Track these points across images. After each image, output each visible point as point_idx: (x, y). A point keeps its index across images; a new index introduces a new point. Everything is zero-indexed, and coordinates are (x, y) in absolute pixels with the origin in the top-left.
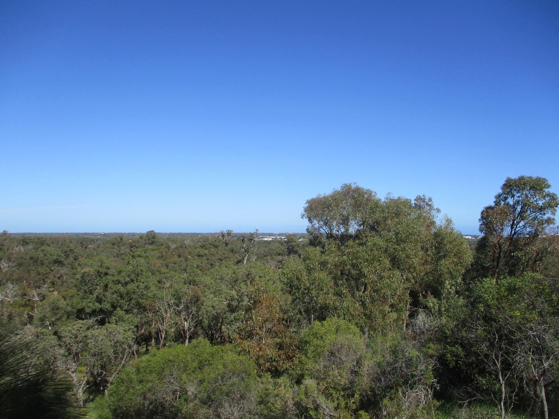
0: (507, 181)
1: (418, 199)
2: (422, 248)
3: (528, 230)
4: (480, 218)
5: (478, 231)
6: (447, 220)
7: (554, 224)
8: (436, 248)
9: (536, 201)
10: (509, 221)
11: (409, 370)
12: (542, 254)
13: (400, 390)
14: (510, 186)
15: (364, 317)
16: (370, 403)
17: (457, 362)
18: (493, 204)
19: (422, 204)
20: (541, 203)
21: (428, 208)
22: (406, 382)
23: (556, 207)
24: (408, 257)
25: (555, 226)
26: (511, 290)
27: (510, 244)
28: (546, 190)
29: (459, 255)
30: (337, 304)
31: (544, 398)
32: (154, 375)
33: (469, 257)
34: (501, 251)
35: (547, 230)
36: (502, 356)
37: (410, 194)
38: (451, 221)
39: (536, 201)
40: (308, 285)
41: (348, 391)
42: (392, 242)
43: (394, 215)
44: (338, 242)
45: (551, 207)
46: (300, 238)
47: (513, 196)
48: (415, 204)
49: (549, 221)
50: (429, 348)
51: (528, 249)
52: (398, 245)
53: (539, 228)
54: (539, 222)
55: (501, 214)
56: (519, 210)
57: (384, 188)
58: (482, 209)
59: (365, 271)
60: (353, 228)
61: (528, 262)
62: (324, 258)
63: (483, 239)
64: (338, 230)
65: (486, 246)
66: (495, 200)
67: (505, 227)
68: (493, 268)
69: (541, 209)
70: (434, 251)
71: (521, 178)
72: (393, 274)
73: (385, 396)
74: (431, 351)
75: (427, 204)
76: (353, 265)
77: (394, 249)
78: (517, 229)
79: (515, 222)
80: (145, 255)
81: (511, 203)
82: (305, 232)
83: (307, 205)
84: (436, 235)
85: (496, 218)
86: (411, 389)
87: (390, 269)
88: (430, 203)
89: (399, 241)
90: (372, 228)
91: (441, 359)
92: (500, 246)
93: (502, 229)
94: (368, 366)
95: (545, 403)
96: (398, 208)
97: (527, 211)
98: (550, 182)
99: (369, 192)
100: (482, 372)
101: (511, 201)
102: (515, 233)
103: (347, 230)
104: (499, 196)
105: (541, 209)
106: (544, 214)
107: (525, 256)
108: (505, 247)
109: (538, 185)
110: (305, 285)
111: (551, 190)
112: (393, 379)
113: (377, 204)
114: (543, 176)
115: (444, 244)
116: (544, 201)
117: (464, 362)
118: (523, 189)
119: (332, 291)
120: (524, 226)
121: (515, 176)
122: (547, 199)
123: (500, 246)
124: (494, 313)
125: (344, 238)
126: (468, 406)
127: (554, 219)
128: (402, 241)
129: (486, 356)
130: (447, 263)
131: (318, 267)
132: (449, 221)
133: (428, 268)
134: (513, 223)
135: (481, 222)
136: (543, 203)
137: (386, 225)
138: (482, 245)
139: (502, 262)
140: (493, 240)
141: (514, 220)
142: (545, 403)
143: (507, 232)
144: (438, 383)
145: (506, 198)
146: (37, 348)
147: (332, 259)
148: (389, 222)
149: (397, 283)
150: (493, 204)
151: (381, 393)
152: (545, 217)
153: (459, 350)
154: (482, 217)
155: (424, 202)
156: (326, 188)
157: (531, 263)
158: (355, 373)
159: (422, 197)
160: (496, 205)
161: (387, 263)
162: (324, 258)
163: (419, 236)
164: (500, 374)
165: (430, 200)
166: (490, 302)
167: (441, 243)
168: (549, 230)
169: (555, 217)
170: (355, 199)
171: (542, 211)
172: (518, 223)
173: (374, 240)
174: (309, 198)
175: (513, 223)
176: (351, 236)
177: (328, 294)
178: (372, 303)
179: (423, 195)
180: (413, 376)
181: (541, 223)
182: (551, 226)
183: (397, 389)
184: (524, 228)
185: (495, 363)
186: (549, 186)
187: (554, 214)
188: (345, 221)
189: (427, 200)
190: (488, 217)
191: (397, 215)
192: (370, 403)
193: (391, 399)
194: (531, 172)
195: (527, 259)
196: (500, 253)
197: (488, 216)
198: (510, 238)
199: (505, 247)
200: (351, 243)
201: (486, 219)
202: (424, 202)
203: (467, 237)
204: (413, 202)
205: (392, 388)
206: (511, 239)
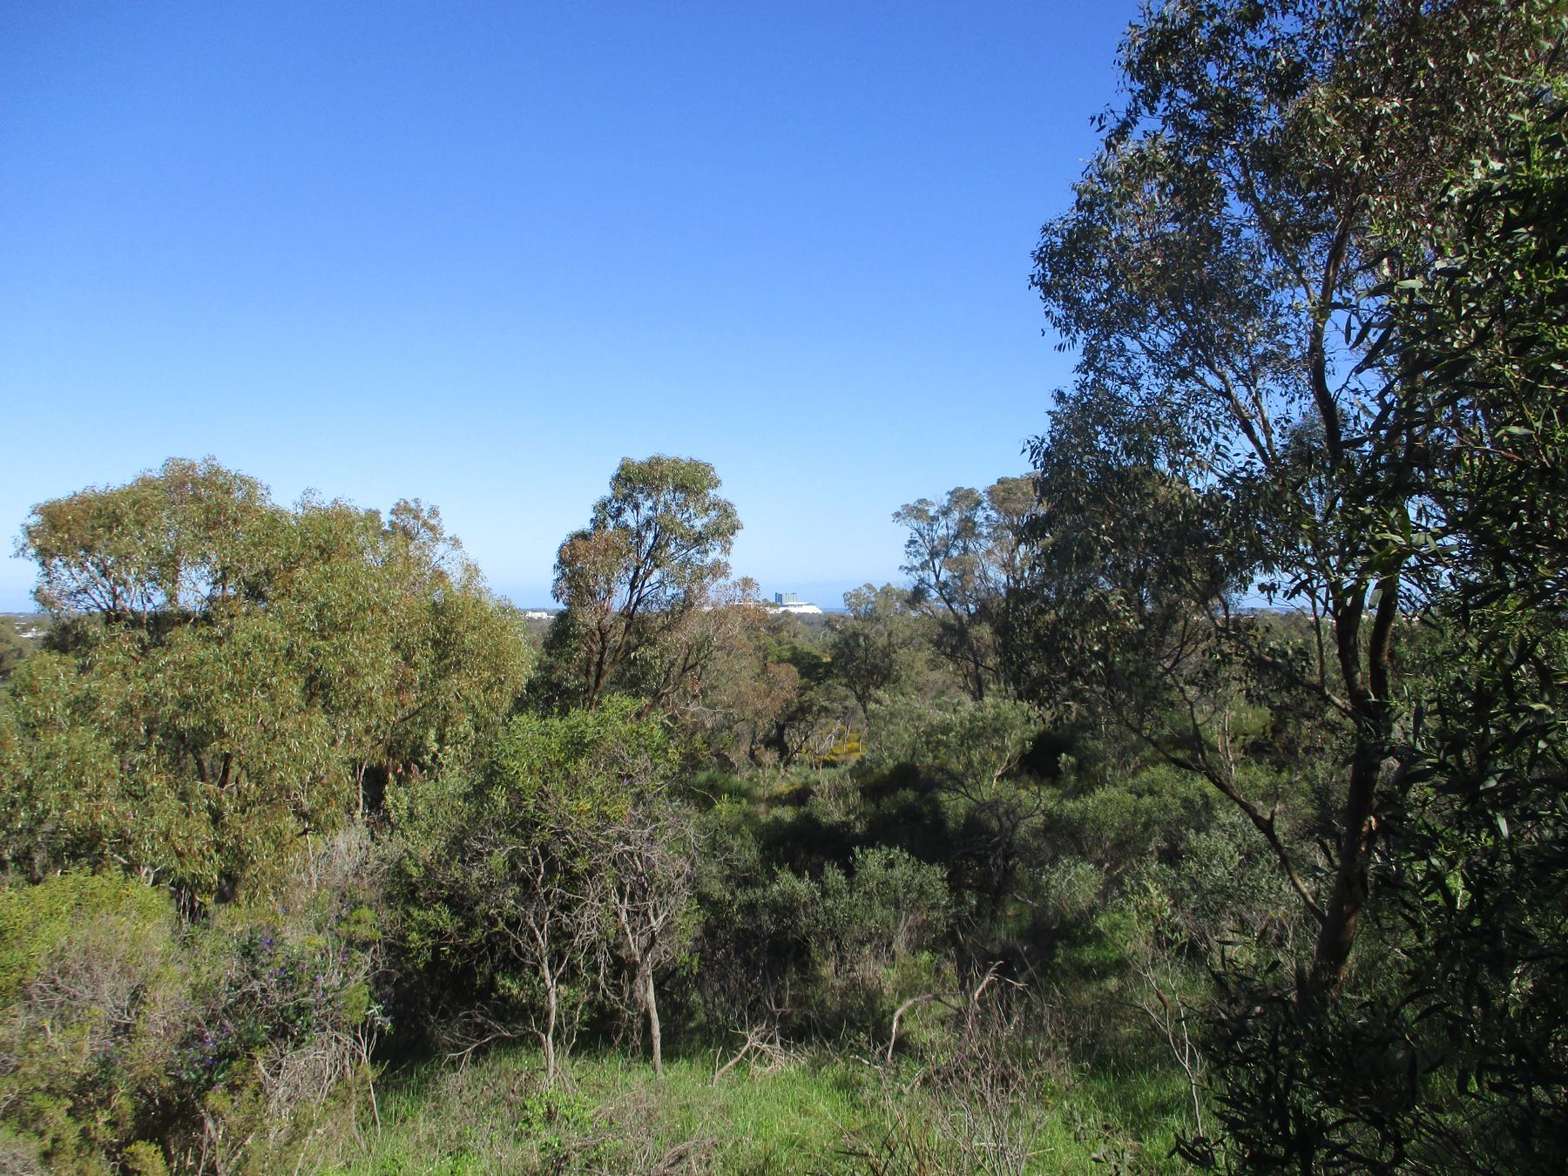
0: (622, 468)
1: (401, 509)
2: (396, 648)
3: (670, 591)
4: (555, 561)
5: (550, 596)
6: (467, 569)
7: (727, 577)
8: (436, 643)
9: (689, 520)
10: (627, 569)
11: (290, 995)
12: (699, 650)
13: (259, 1054)
14: (633, 481)
15: (217, 857)
16: (169, 1118)
17: (436, 950)
18: (588, 526)
19: (410, 526)
20: (698, 524)
21: (431, 534)
22: (281, 1032)
24: (351, 671)
25: (729, 583)
26: (577, 747)
27: (628, 627)
28: (712, 492)
29: (497, 662)
30: (130, 826)
31: (653, 1005)
33: (524, 666)
34: (604, 648)
36: (552, 915)
37: (373, 494)
38: (477, 571)
39: (689, 520)
40: (27, 773)
41: (86, 1093)
42: (307, 630)
43: (316, 553)
44: (144, 634)
46: (25, 630)
47: (637, 507)
48: (392, 524)
49: (718, 570)
50: (358, 922)
51: (669, 639)
52: (324, 638)
53: (695, 587)
55: (606, 550)
56: (650, 541)
57: (295, 473)
58: (561, 537)
59: (225, 715)
60: (194, 588)
61: (667, 673)
62: (89, 684)
63: (562, 616)
64: (145, 599)
65: (567, 636)
66: (593, 516)
67: (616, 586)
68: (586, 691)
69: (699, 539)
70: (430, 652)
71: (655, 462)
72: (310, 724)
73: (211, 1084)
74: (363, 932)
75: (425, 524)
76: (186, 704)
77: (312, 651)
78: (645, 591)
79: (641, 571)
81: (633, 524)
82: (31, 607)
83: (36, 519)
84: (437, 610)
85: (594, 563)
86: (296, 1047)
87: (301, 710)
88: (433, 522)
89: (327, 627)
90: (254, 592)
91: (397, 949)
92: (603, 636)
93: (609, 591)
94: (169, 1003)
95: (654, 1015)
96: (328, 536)
97: (667, 545)
98: (720, 472)
99: (249, 484)
100: (513, 965)
101: (630, 518)
102: (639, 601)
103: (172, 598)
104: (603, 506)
105: (699, 539)
107: (662, 656)
108: (616, 638)
109: (691, 481)
110: (16, 774)
111: (721, 494)
112: (252, 1024)
113: (275, 519)
114: (702, 456)
115: (458, 634)
116: (706, 520)
117: (456, 948)
118: (658, 489)
119: (111, 788)
120: (661, 582)
121: (640, 455)
123: (603, 636)
124: (531, 808)
125: (160, 624)
126: (475, 1062)
127: (727, 565)
128: (335, 627)
129: (513, 924)
130: (464, 684)
131: (61, 714)
132: (472, 571)
133: (412, 699)
134: (636, 573)
135: (558, 574)
137: (292, 581)
138: (561, 633)
139: (610, 672)
140: (587, 618)
141: (638, 569)
142: (654, 1015)
143: (620, 597)
144: (385, 1013)
145: (620, 511)
147: (111, 692)
148: (301, 572)
149: (324, 748)
150: (588, 526)
151: (199, 1078)
152: (709, 560)
153: (442, 917)
154: (562, 561)
155: (416, 517)
156: (111, 466)
157: (675, 671)
158: (124, 1030)
159: (413, 505)
160: (596, 527)
161: (294, 691)
162: (89, 684)
163: (385, 611)
164: (546, 965)
165: (434, 512)
166: (525, 780)
167: (448, 630)
168: (716, 593)
169: (731, 560)
170: (204, 504)
172: (648, 574)
173: (260, 625)
174: (43, 498)
175: (636, 573)
176: (186, 617)
177: (98, 797)
178: (243, 812)
179: (416, 500)
180: (300, 1010)
181: (699, 575)
182: (721, 581)
183: (250, 1056)
184: (661, 588)
185: (534, 939)
186: (717, 484)
188: (167, 568)
189: (425, 514)
190: (576, 565)
191: (325, 552)
192: (169, 1118)
193: (233, 1088)
194: (676, 446)
195: (666, 666)
196: (602, 654)
197: (575, 558)
198: (628, 614)
199: (616, 638)
200: (183, 634)
201: (569, 564)
202: (416, 517)
203: (536, 615)
204: (386, 518)
205: (234, 1056)
206: (631, 616)
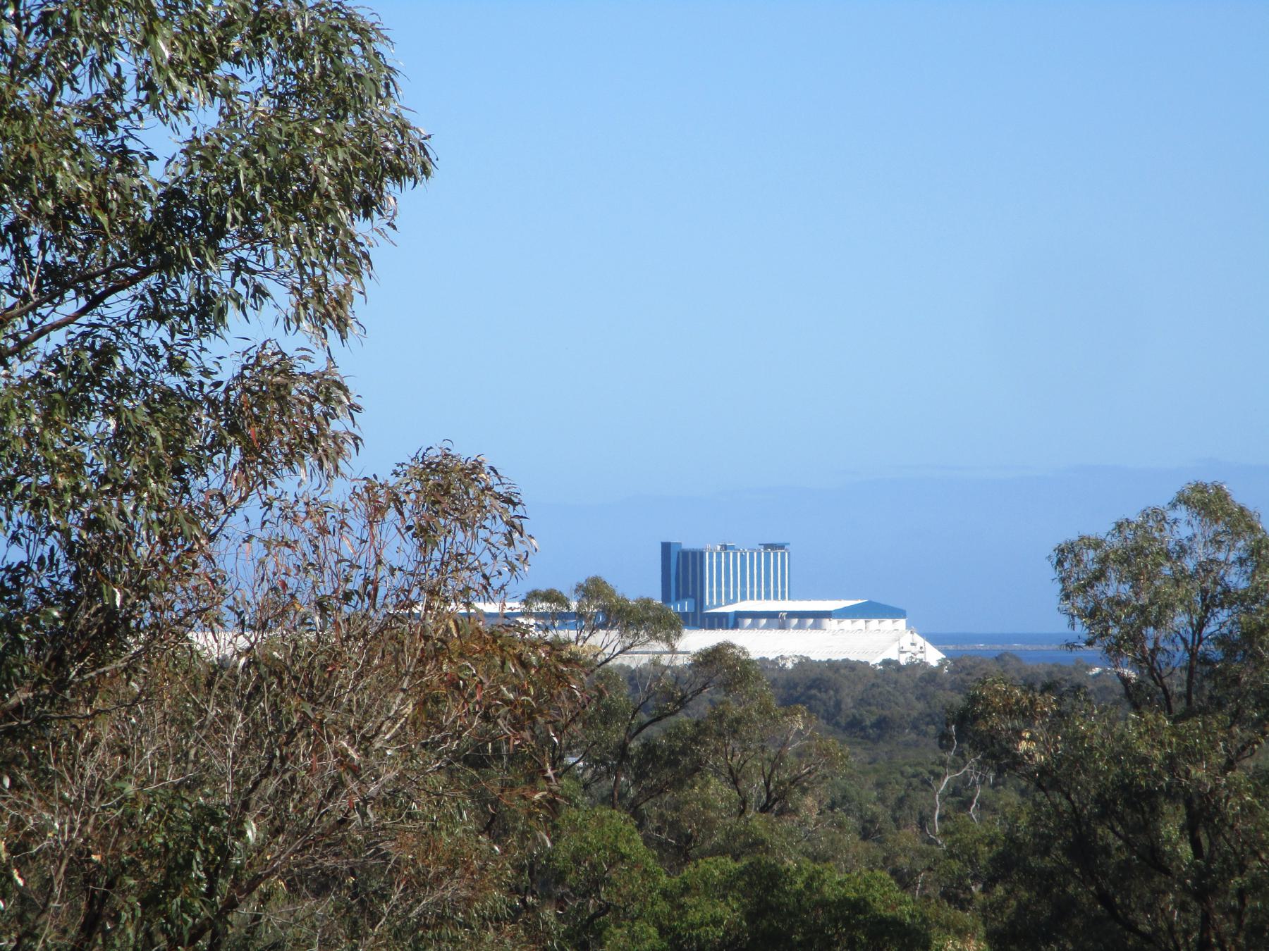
9: (100, 117)
20: (161, 144)
23: (367, 205)
32: (1184, 531)
35: (240, 553)
45: (292, 208)
54: (125, 439)
80: (924, 727)
106: (208, 311)
116: (206, 116)
122: (252, 80)
127: (329, 390)
136: (200, 152)
146: (305, 847)
152: (223, 354)
169: (352, 360)
171: (170, 264)
181: (169, 436)
182: (296, 483)
187: (331, 313)
